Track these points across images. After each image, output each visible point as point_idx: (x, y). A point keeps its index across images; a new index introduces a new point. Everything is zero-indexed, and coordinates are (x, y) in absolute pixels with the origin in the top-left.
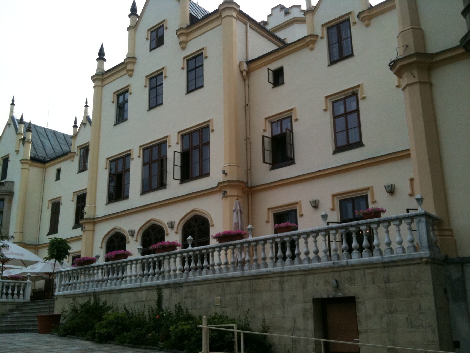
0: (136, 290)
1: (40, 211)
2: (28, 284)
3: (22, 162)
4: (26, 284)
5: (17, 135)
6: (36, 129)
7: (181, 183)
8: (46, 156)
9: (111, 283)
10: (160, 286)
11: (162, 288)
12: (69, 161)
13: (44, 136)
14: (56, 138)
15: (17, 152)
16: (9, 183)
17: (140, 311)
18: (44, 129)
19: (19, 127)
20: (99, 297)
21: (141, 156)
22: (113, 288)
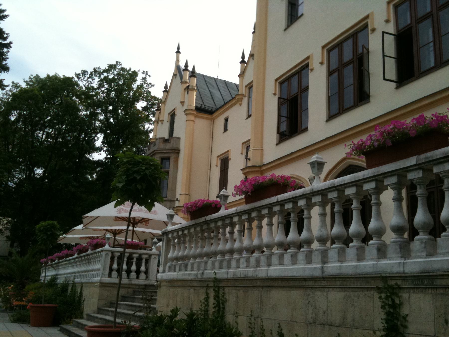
0: (310, 284)
1: (209, 170)
2: (153, 257)
3: (187, 112)
4: (150, 255)
5: (182, 84)
6: (205, 79)
7: (397, 88)
8: (214, 106)
9: (248, 260)
10: (392, 278)
11: (400, 288)
12: (237, 106)
13: (213, 86)
14: (227, 89)
15: (182, 103)
16: (175, 139)
18: (215, 79)
19: (184, 73)
20: (224, 293)
21: (325, 62)
22: (250, 272)
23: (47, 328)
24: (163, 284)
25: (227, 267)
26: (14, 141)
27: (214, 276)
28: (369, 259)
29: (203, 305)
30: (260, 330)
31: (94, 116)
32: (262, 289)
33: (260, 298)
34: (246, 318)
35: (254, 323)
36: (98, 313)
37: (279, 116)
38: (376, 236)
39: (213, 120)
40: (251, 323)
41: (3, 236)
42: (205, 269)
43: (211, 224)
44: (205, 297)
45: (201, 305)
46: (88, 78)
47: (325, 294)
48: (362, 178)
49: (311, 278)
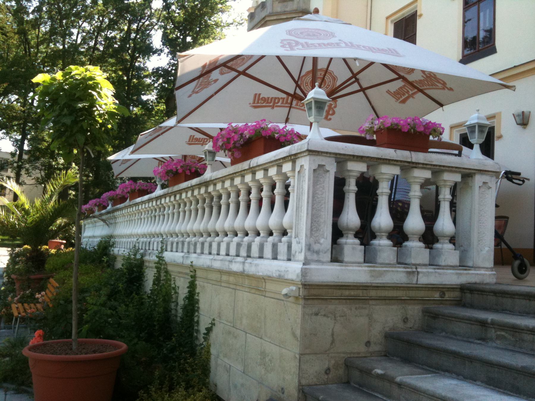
2: (478, 179)
41: (31, 178)
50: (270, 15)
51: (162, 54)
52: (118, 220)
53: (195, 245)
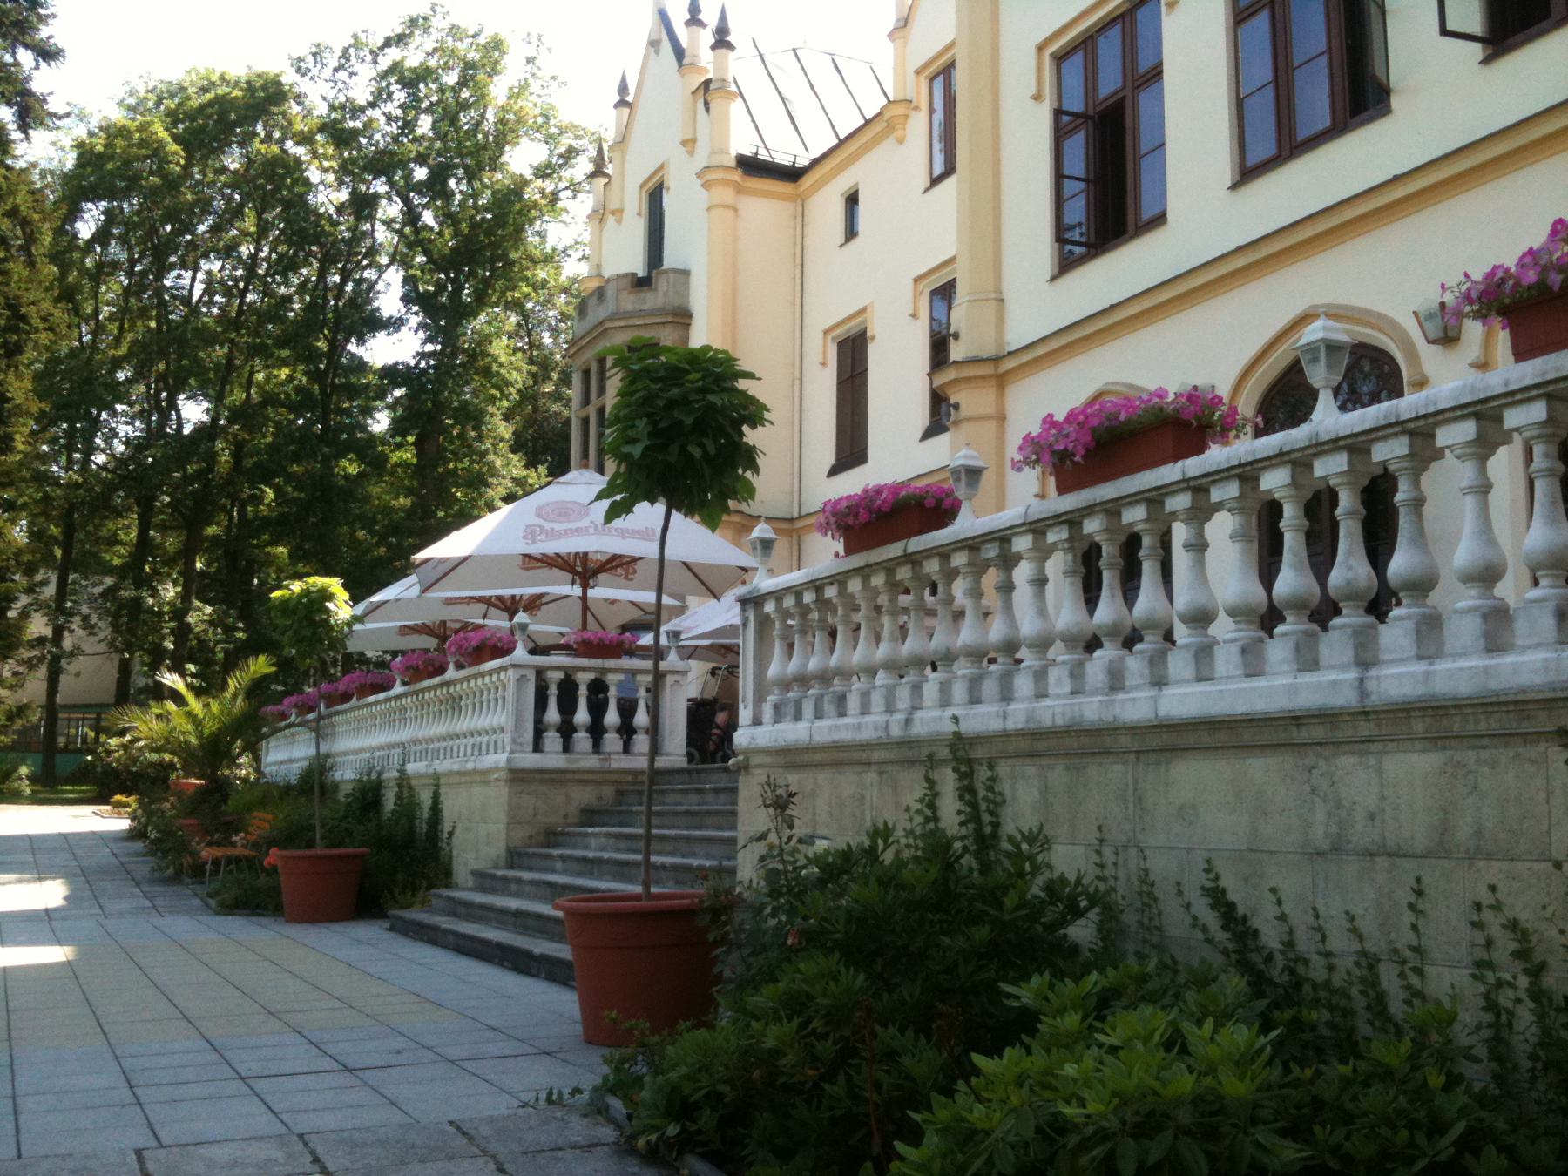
1: (797, 383)
9: (1077, 673)
17: (1370, 947)
20: (993, 779)
23: (345, 923)
24: (755, 760)
25: (997, 697)
26: (97, 312)
27: (950, 727)
28: (1530, 647)
29: (919, 819)
30: (1137, 883)
31: (363, 206)
32: (1138, 758)
33: (1131, 786)
34: (1080, 850)
35: (1115, 864)
36: (511, 867)
37: (1059, 176)
38: (1549, 572)
39: (803, 201)
40: (1102, 866)
41: (97, 638)
42: (915, 708)
43: (925, 563)
44: (926, 795)
45: (911, 820)
46: (336, 70)
47: (1372, 761)
48: (1501, 390)
49: (1319, 716)
50: (611, 318)
51: (404, 329)
52: (340, 729)
53: (438, 751)
